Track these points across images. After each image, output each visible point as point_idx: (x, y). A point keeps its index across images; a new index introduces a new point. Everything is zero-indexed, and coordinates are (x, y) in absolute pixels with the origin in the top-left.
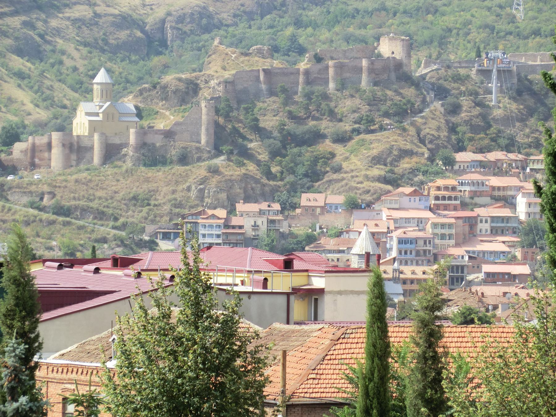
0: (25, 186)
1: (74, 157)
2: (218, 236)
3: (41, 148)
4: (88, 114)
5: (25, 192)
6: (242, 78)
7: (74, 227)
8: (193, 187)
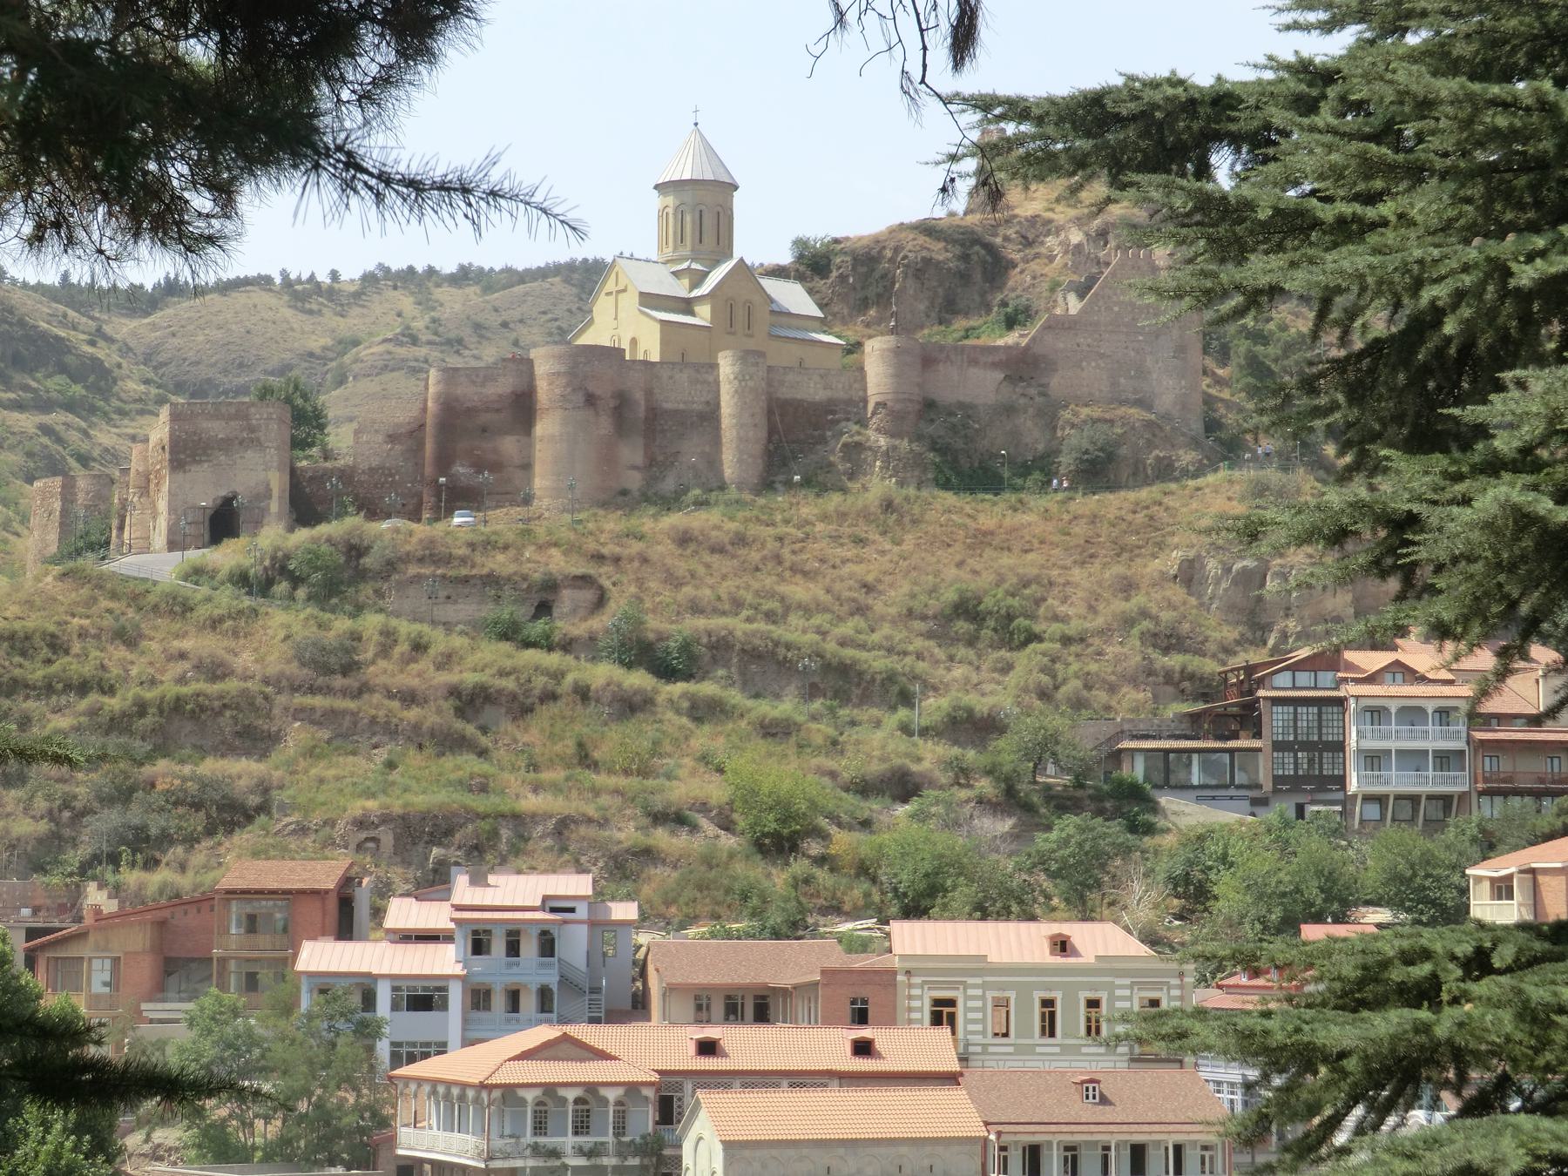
0: (463, 551)
1: (632, 453)
2: (1445, 759)
3: (485, 418)
5: (466, 580)
7: (743, 724)
8: (1212, 566)
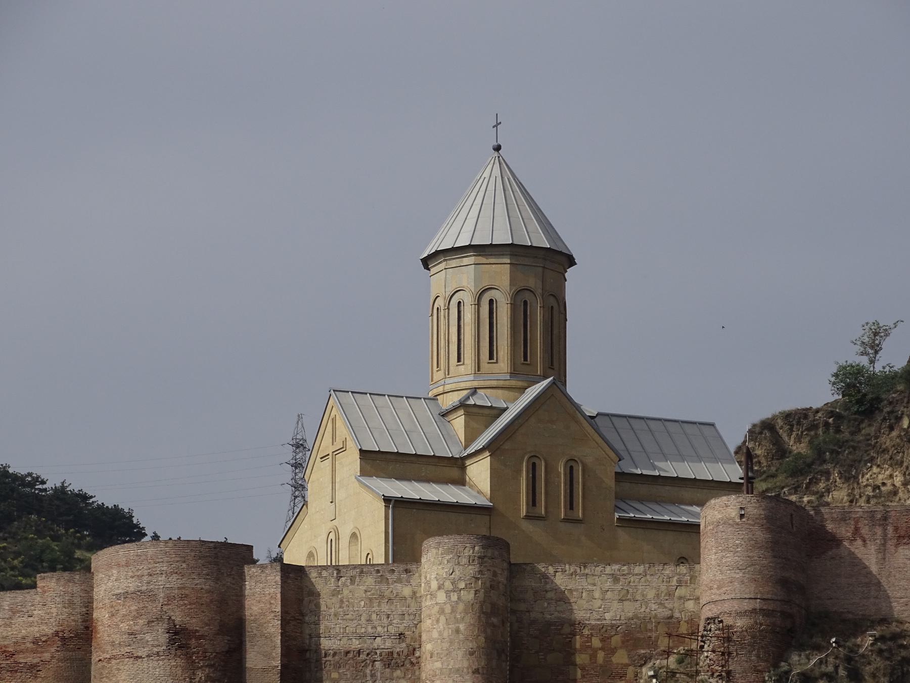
4: (375, 462)
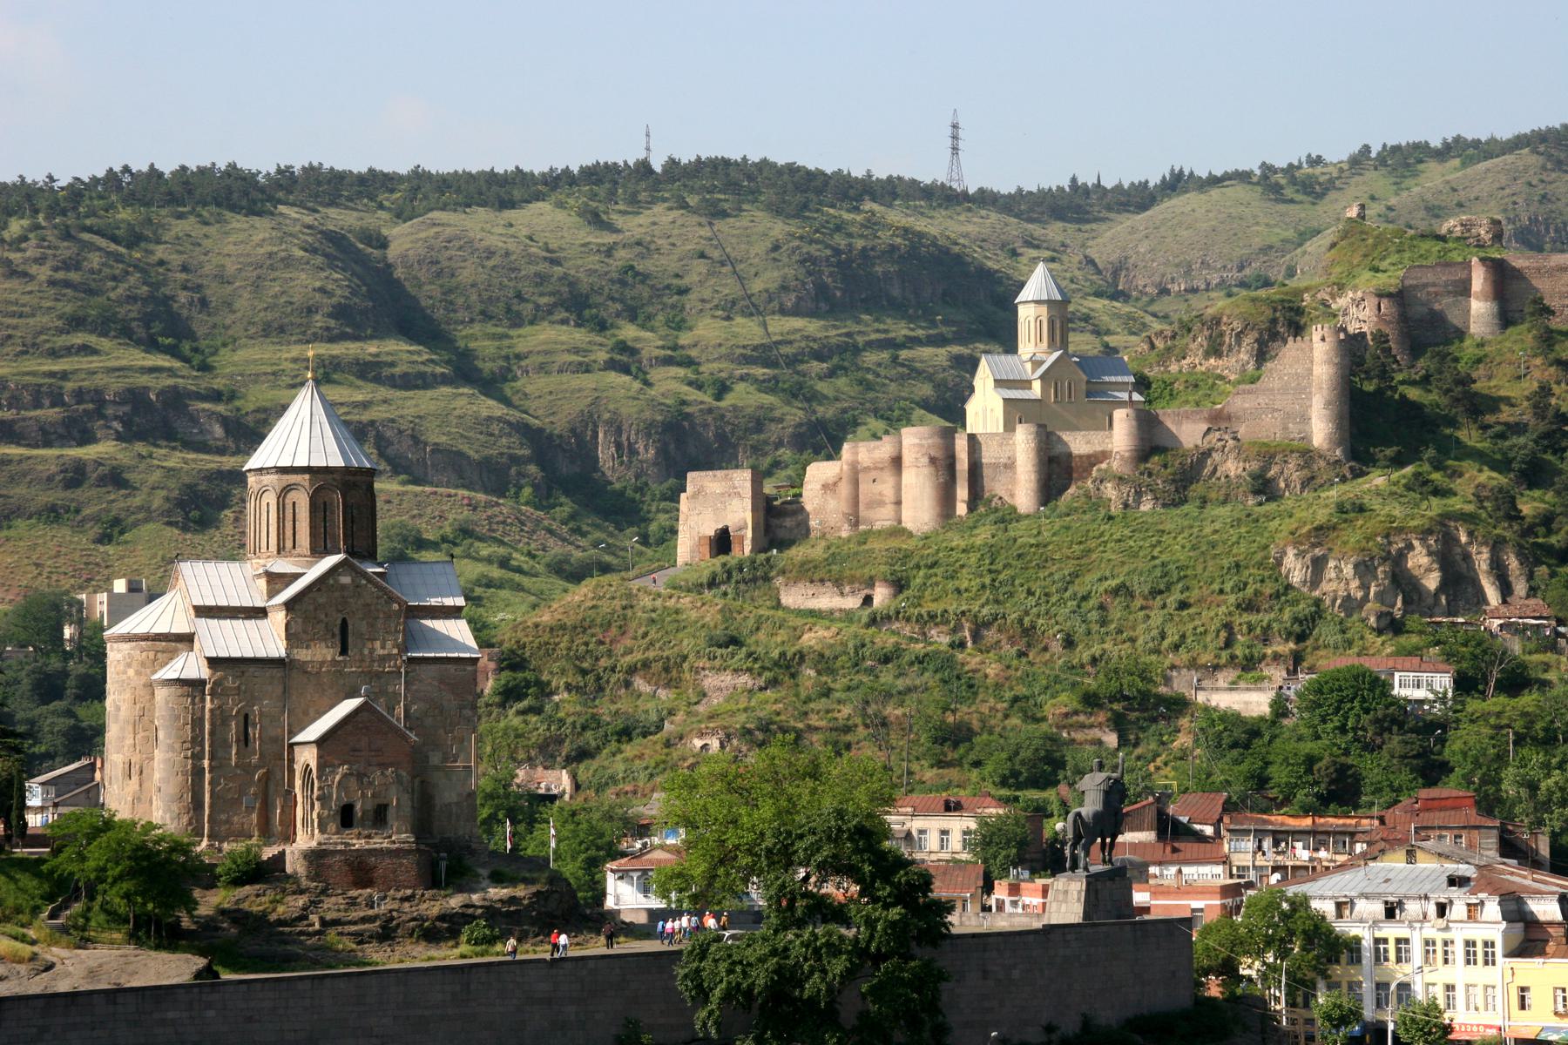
6: (1425, 285)
